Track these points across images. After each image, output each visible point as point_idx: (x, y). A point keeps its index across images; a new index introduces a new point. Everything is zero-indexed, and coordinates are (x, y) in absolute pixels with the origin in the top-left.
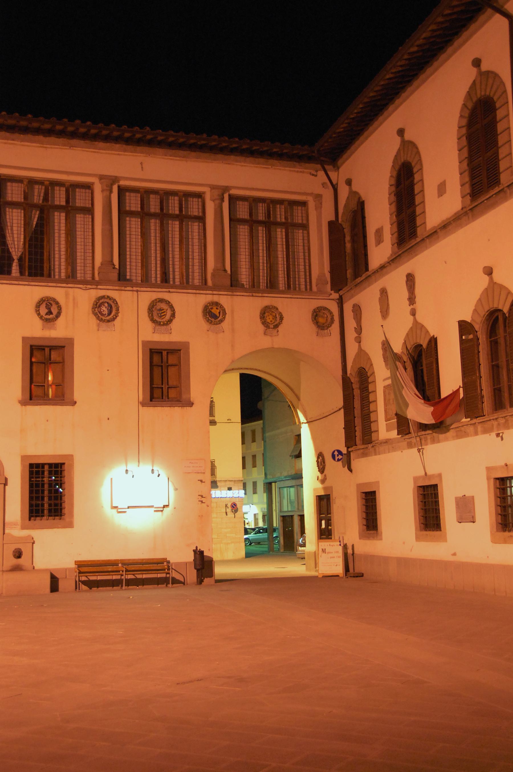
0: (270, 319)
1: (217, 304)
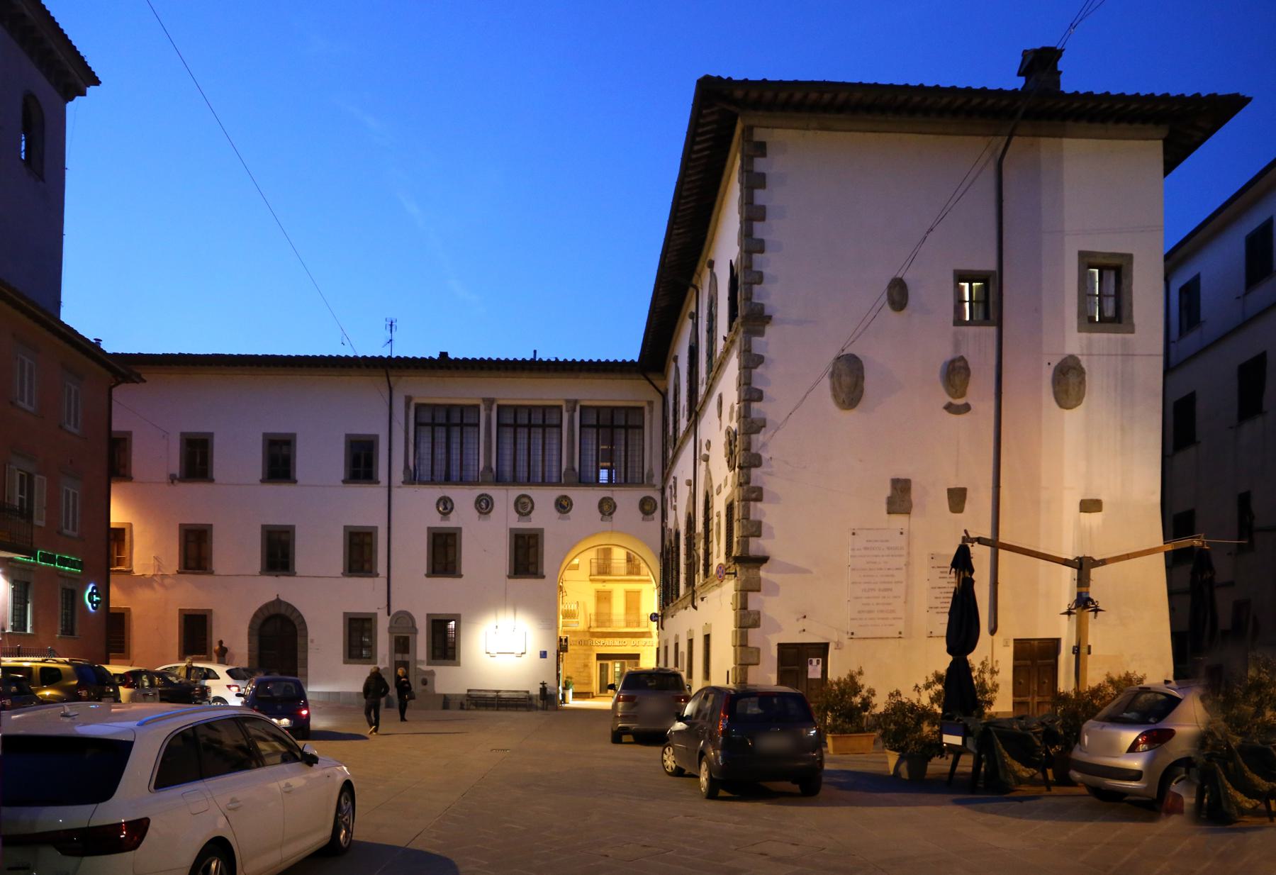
1: (565, 497)
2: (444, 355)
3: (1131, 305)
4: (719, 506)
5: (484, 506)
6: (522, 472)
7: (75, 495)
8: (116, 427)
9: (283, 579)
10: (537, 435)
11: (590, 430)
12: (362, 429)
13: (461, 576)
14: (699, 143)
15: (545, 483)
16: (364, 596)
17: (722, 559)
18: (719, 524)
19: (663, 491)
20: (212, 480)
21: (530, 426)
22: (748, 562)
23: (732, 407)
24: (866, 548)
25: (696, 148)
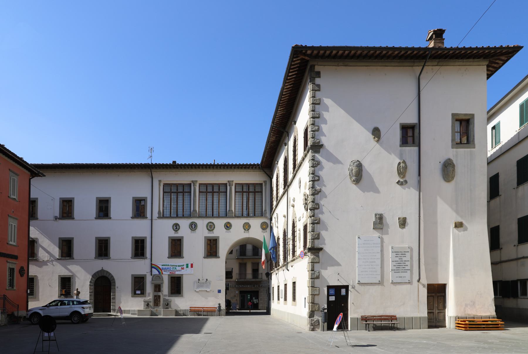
0: (247, 227)
1: (228, 223)
2: (174, 162)
3: (474, 136)
4: (300, 227)
5: (193, 227)
6: (209, 212)
7: (15, 226)
8: (33, 196)
12: (140, 195)
13: (219, 257)
14: (292, 72)
16: (141, 267)
17: (302, 249)
18: (300, 234)
19: (271, 219)
20: (73, 219)
22: (315, 250)
23: (306, 184)
24: (364, 244)
25: (290, 74)
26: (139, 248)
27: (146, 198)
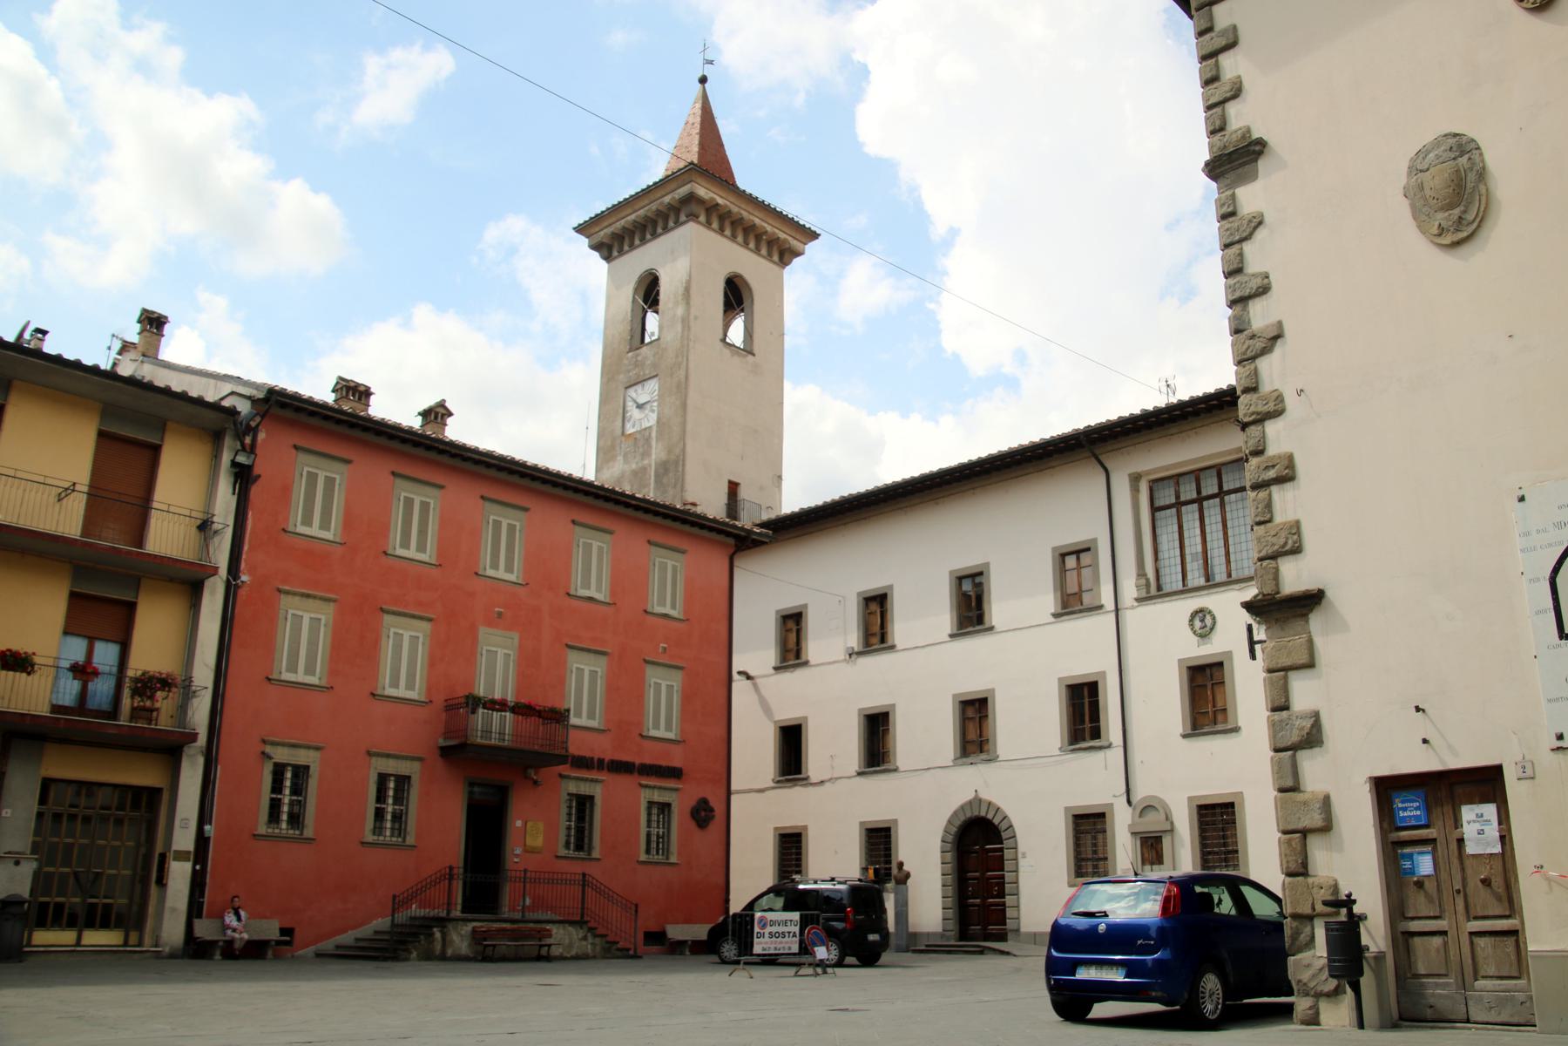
7: (670, 687)
9: (983, 768)
10: (1190, 515)
11: (1189, 507)
15: (1230, 582)
16: (1092, 779)
21: (1200, 500)
26: (1083, 710)
27: (1095, 541)
